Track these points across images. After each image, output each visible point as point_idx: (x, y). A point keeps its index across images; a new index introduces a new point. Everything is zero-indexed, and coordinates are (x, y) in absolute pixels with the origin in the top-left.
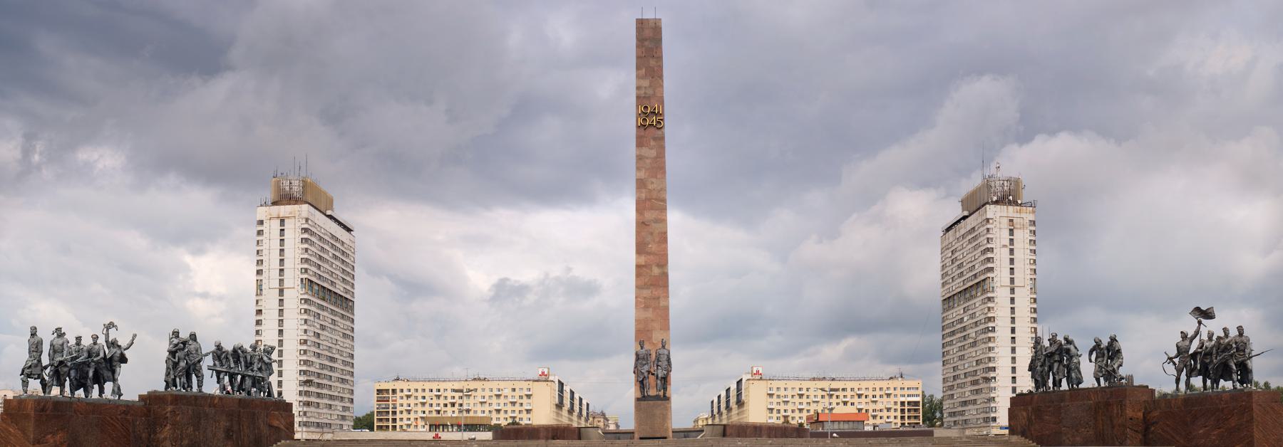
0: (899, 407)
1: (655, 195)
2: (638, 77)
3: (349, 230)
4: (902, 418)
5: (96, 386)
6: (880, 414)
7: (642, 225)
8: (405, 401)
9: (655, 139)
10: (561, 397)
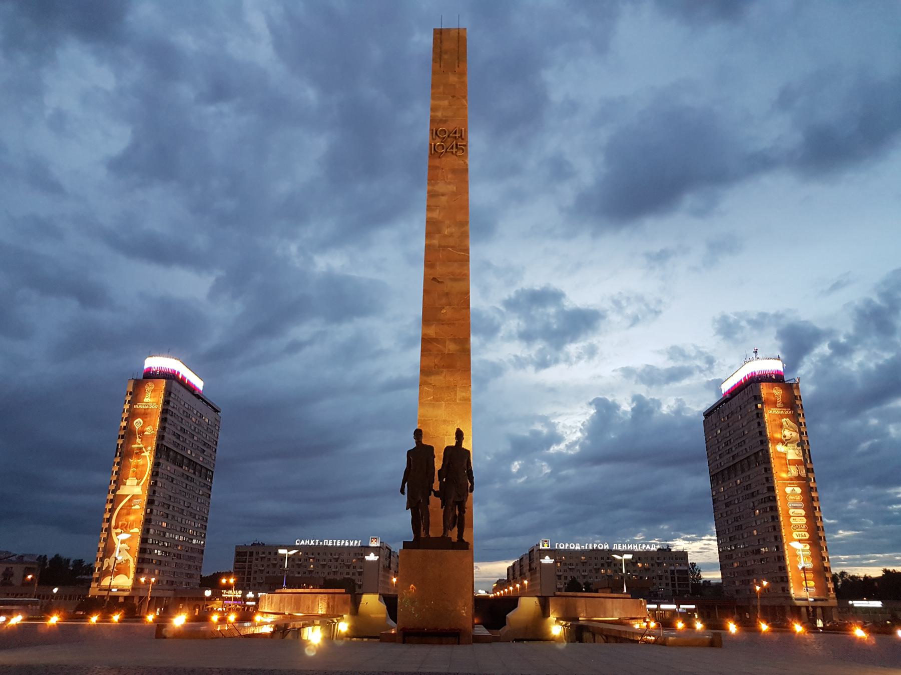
0: (668, 575)
2: (434, 97)
4: (673, 585)
5: (281, 551)
9: (454, 171)
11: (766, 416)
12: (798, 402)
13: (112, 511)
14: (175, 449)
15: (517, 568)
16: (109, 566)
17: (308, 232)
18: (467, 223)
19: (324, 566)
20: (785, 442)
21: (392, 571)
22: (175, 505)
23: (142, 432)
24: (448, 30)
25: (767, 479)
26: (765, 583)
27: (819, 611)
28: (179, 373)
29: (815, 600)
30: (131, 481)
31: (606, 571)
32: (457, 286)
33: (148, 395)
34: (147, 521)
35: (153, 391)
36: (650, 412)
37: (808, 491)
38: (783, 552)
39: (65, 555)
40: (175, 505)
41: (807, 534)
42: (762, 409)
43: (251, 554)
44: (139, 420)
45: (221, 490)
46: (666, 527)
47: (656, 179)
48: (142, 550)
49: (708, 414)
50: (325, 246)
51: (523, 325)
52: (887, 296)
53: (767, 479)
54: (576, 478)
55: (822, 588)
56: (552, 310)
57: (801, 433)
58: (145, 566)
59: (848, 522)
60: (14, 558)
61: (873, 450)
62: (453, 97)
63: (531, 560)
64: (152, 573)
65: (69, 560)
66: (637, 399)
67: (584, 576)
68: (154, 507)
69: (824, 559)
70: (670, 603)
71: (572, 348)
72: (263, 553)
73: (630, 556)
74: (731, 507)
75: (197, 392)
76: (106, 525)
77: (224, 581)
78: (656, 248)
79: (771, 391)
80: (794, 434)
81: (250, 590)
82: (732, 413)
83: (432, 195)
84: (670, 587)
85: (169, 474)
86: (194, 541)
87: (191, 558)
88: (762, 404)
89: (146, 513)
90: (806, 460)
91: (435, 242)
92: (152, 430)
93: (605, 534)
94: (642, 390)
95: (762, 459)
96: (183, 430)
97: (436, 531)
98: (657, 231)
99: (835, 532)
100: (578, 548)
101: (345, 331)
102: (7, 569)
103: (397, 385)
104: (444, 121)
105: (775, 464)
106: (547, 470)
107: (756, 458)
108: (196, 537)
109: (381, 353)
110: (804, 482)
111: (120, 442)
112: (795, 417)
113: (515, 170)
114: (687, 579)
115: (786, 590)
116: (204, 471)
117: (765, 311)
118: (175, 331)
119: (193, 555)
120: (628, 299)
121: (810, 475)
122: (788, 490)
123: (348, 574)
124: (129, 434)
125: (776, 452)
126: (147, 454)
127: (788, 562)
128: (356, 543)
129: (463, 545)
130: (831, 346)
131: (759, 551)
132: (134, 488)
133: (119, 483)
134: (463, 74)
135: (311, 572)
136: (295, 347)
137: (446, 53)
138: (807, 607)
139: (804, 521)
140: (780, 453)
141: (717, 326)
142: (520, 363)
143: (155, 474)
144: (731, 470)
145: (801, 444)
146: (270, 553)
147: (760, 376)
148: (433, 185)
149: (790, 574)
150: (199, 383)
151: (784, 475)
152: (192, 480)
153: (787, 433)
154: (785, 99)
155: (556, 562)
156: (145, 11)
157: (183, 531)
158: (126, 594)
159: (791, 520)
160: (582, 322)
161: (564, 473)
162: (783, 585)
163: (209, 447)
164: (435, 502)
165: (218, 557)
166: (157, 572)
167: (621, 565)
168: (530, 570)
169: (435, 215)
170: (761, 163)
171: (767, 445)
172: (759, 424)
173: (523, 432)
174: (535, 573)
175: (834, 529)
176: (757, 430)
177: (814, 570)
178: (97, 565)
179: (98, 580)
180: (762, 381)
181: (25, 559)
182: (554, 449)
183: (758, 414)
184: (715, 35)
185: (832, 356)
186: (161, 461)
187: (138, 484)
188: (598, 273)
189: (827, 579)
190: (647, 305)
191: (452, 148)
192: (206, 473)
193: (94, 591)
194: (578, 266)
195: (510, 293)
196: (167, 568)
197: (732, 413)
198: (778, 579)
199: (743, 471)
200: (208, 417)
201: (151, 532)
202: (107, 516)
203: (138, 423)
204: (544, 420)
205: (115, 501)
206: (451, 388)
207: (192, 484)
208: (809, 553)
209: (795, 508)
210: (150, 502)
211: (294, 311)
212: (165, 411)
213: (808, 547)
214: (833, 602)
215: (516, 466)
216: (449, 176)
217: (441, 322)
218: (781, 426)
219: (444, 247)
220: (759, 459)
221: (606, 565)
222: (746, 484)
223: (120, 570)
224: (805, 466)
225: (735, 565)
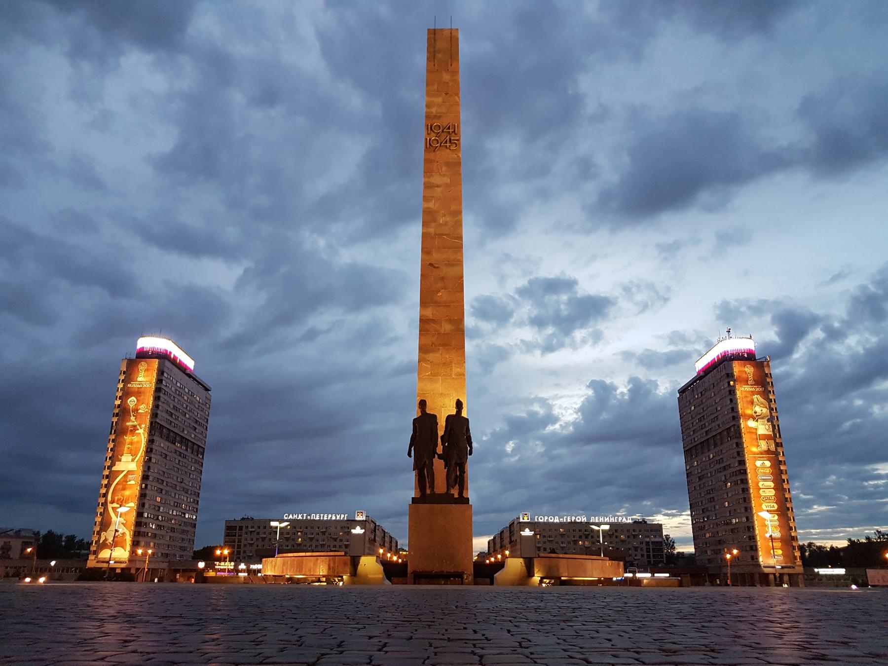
0: (644, 546)
2: (428, 94)
4: (648, 557)
5: (273, 524)
7: (429, 269)
8: (248, 536)
9: (447, 164)
10: (842, 642)
12: (768, 380)
13: (107, 486)
14: (168, 426)
15: (498, 541)
16: (106, 540)
17: (336, 228)
19: (311, 539)
20: (755, 418)
21: (377, 544)
22: (168, 480)
23: (136, 410)
24: (441, 30)
25: (738, 453)
26: (735, 552)
27: (786, 578)
28: (170, 353)
29: (783, 567)
30: (126, 458)
31: (584, 543)
33: (142, 374)
34: (143, 495)
35: (147, 370)
36: (648, 393)
37: (777, 464)
38: (753, 522)
39: (57, 531)
40: (168, 480)
41: (776, 505)
42: (734, 386)
43: (241, 528)
44: (133, 398)
45: (212, 469)
46: (649, 503)
47: (674, 177)
48: (138, 524)
49: (682, 391)
50: (352, 241)
51: (535, 312)
52: (879, 283)
53: (738, 453)
54: (567, 457)
55: (789, 556)
56: (564, 297)
57: (771, 409)
58: (141, 539)
59: (824, 498)
60: (11, 533)
61: (855, 429)
62: (446, 94)
63: (511, 533)
64: (147, 546)
65: (61, 536)
66: (634, 381)
68: (148, 483)
69: (791, 529)
70: (646, 571)
71: (579, 334)
72: (252, 527)
74: (704, 480)
75: (188, 372)
76: (102, 500)
78: (669, 239)
80: (765, 410)
81: (241, 562)
82: (706, 390)
83: (428, 186)
85: (164, 451)
88: (735, 381)
89: (141, 488)
91: (431, 230)
92: (145, 408)
93: (586, 510)
94: (642, 374)
96: (175, 408)
97: (440, 486)
98: (673, 225)
99: (810, 507)
100: (557, 520)
101: (363, 318)
103: (403, 370)
104: (438, 117)
105: (746, 438)
106: (540, 449)
107: (728, 434)
108: (189, 511)
109: (395, 339)
110: (773, 456)
111: (115, 419)
112: (765, 394)
113: (543, 170)
114: (661, 550)
115: (755, 558)
116: (195, 447)
117: (766, 298)
118: (192, 316)
119: (185, 528)
120: (638, 286)
121: (779, 449)
122: (758, 463)
124: (123, 412)
125: (747, 427)
126: (141, 431)
127: (757, 532)
128: (343, 517)
130: (823, 330)
131: (730, 523)
132: (129, 464)
133: (115, 459)
134: (456, 72)
135: (300, 545)
136: (312, 335)
138: (774, 574)
139: (773, 492)
140: (751, 428)
141: (718, 312)
142: (529, 347)
143: (149, 450)
144: (705, 445)
145: (771, 420)
147: (733, 355)
148: (429, 177)
149: (759, 543)
150: (190, 363)
151: (754, 449)
152: (185, 457)
153: (758, 409)
154: (807, 108)
155: (535, 535)
156: (205, 24)
157: (177, 505)
158: (123, 565)
159: (761, 491)
160: (591, 309)
161: (555, 452)
162: (753, 553)
163: (200, 424)
164: (439, 465)
165: (209, 532)
166: (152, 544)
167: (599, 537)
168: (511, 542)
169: (431, 205)
170: (774, 162)
171: (739, 421)
172: (731, 400)
173: (521, 413)
175: (808, 504)
178: (95, 539)
179: (95, 553)
180: (734, 359)
181: (23, 533)
182: (550, 428)
183: (730, 391)
184: (749, 48)
185: (824, 340)
186: (155, 438)
187: (133, 460)
188: (610, 262)
189: (794, 548)
190: (657, 292)
191: (446, 142)
192: (198, 450)
193: (91, 563)
194: (594, 258)
195: (522, 282)
196: (161, 541)
197: (706, 390)
198: (748, 549)
199: (716, 446)
202: (103, 491)
203: (132, 401)
204: (543, 402)
205: (111, 477)
206: (447, 364)
207: (185, 460)
208: (777, 523)
210: (145, 478)
211: (316, 300)
212: (158, 390)
213: (776, 517)
214: (799, 569)
215: (510, 447)
217: (437, 304)
218: (752, 403)
219: (440, 235)
220: (732, 434)
221: (583, 537)
222: (718, 458)
223: (117, 542)
224: (775, 441)
225: (708, 535)
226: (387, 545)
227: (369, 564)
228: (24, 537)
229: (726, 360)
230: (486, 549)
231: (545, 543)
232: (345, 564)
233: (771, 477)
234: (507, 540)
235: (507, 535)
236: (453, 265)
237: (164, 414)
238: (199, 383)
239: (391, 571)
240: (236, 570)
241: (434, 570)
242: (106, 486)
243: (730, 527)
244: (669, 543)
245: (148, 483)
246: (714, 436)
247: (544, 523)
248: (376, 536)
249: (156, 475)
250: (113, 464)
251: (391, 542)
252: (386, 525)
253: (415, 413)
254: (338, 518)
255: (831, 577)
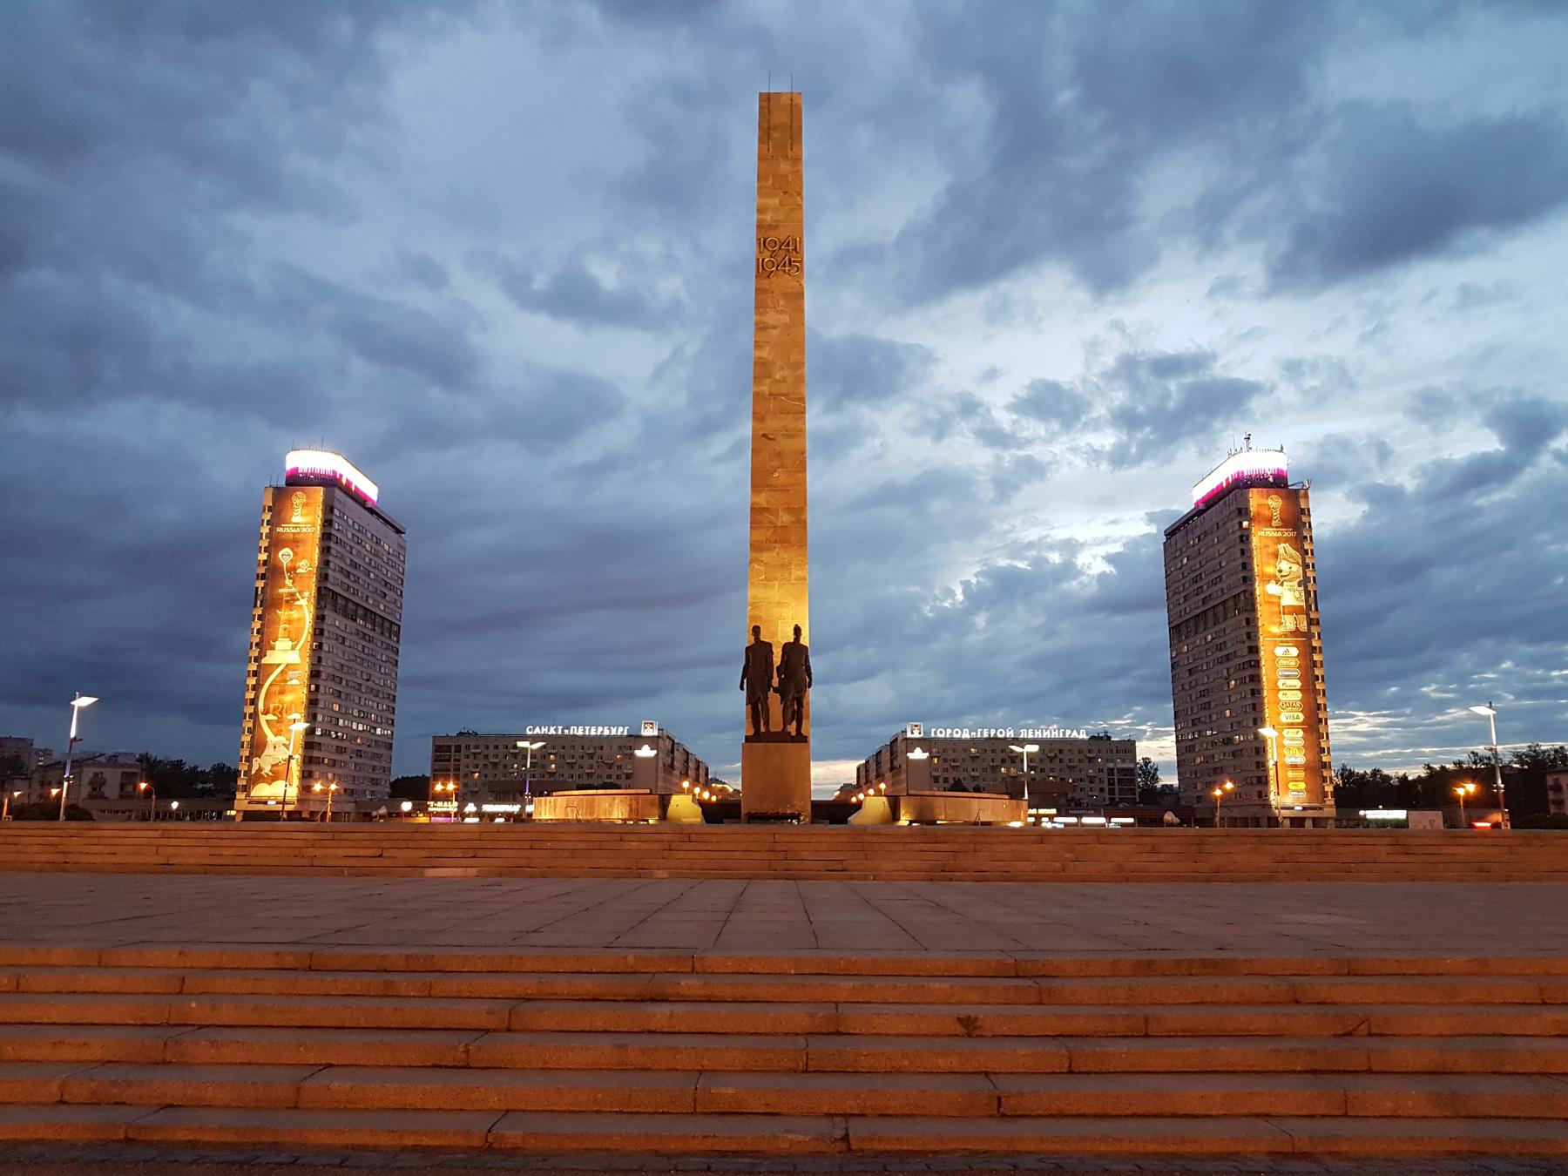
0: (1105, 775)
1: (784, 388)
3: (399, 532)
4: (1112, 791)
5: (520, 744)
6: (580, 762)
7: (762, 439)
8: (471, 761)
9: (786, 296)
11: (1255, 540)
12: (1304, 519)
15: (873, 766)
16: (260, 769)
18: (803, 364)
19: (571, 765)
21: (676, 773)
25: (1249, 635)
26: (1229, 786)
29: (1304, 809)
30: (282, 644)
32: (791, 445)
34: (312, 702)
35: (306, 505)
37: (1308, 651)
42: (1248, 529)
43: (458, 749)
44: (286, 550)
45: (413, 659)
53: (1249, 635)
58: (314, 768)
60: (102, 759)
67: (974, 778)
68: (320, 682)
72: (477, 747)
73: (1034, 748)
75: (369, 505)
76: (250, 709)
77: (439, 787)
79: (1264, 501)
80: (1295, 568)
82: (1206, 533)
83: (761, 327)
84: (1106, 794)
86: (378, 731)
87: (376, 756)
88: (1250, 520)
90: (1309, 607)
92: (308, 564)
95: (1244, 603)
96: (355, 565)
97: (776, 725)
100: (966, 735)
102: (96, 774)
104: (773, 227)
105: (1262, 611)
110: (1303, 639)
111: (260, 584)
114: (1133, 781)
115: (1263, 795)
116: (387, 624)
121: (1314, 630)
122: (1279, 651)
123: (609, 777)
124: (273, 572)
126: (303, 602)
128: (622, 731)
129: (801, 739)
131: (1229, 741)
132: (289, 654)
133: (264, 646)
137: (775, 129)
139: (1299, 695)
143: (318, 632)
146: (496, 747)
148: (761, 314)
150: (371, 490)
151: (1275, 629)
153: (1284, 566)
155: (931, 757)
158: (289, 808)
159: (1280, 695)
162: (1260, 788)
163: (392, 588)
164: (774, 700)
168: (892, 769)
169: (765, 353)
172: (1243, 552)
174: (899, 773)
176: (1241, 561)
177: (1307, 768)
178: (243, 767)
179: (246, 789)
180: (1252, 486)
187: (293, 648)
197: (1206, 533)
200: (389, 541)
201: (320, 718)
202: (250, 695)
203: (285, 556)
206: (785, 566)
208: (1302, 743)
209: (1288, 677)
210: (314, 675)
212: (326, 536)
213: (1301, 733)
214: (1330, 810)
216: (782, 302)
217: (773, 488)
218: (1276, 555)
220: (1241, 605)
222: (1218, 641)
226: (691, 773)
227: (684, 806)
228: (123, 766)
229: (1241, 485)
230: (854, 782)
231: (945, 770)
232: (652, 804)
233: (1297, 673)
234: (886, 766)
235: (886, 757)
236: (792, 436)
237: (338, 575)
238: (386, 522)
239: (719, 812)
240: (461, 814)
241: (763, 813)
242: (254, 688)
243: (1231, 748)
244: (1149, 771)
245: (320, 682)
246: (1214, 607)
247: (945, 739)
248: (678, 762)
249: (331, 671)
250: (262, 655)
251: (698, 769)
252: (697, 749)
253: (749, 640)
254: (614, 732)
255: (1383, 824)
